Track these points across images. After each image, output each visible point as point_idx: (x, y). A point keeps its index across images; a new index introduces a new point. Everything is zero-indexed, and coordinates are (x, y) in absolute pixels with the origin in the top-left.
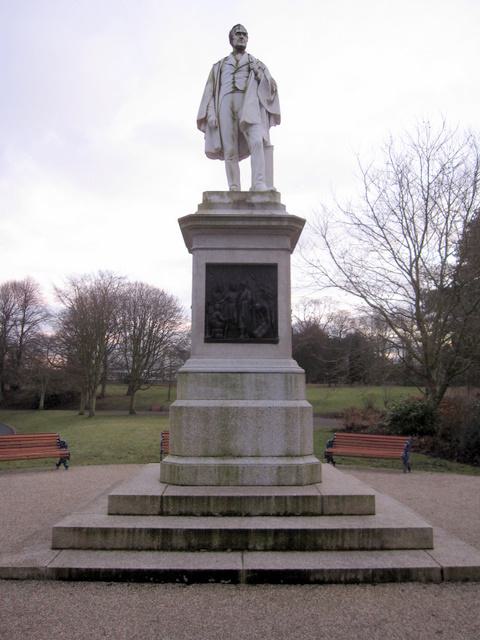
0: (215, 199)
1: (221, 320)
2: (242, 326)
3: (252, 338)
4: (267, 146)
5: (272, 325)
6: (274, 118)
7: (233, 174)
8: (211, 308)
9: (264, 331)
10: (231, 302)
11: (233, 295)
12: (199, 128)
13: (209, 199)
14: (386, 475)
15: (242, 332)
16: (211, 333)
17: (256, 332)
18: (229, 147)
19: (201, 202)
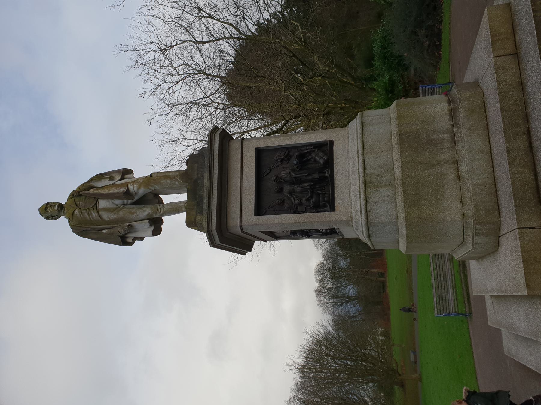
0: (292, 231)
1: (311, 197)
2: (316, 176)
3: (329, 163)
4: (152, 178)
5: (315, 148)
6: (126, 172)
7: (174, 209)
8: (299, 208)
9: (321, 154)
10: (294, 189)
11: (287, 188)
12: (130, 244)
13: (191, 223)
14: (336, 202)
15: (322, 174)
16: (325, 206)
17: (322, 161)
18: (146, 211)
19: (72, 230)
